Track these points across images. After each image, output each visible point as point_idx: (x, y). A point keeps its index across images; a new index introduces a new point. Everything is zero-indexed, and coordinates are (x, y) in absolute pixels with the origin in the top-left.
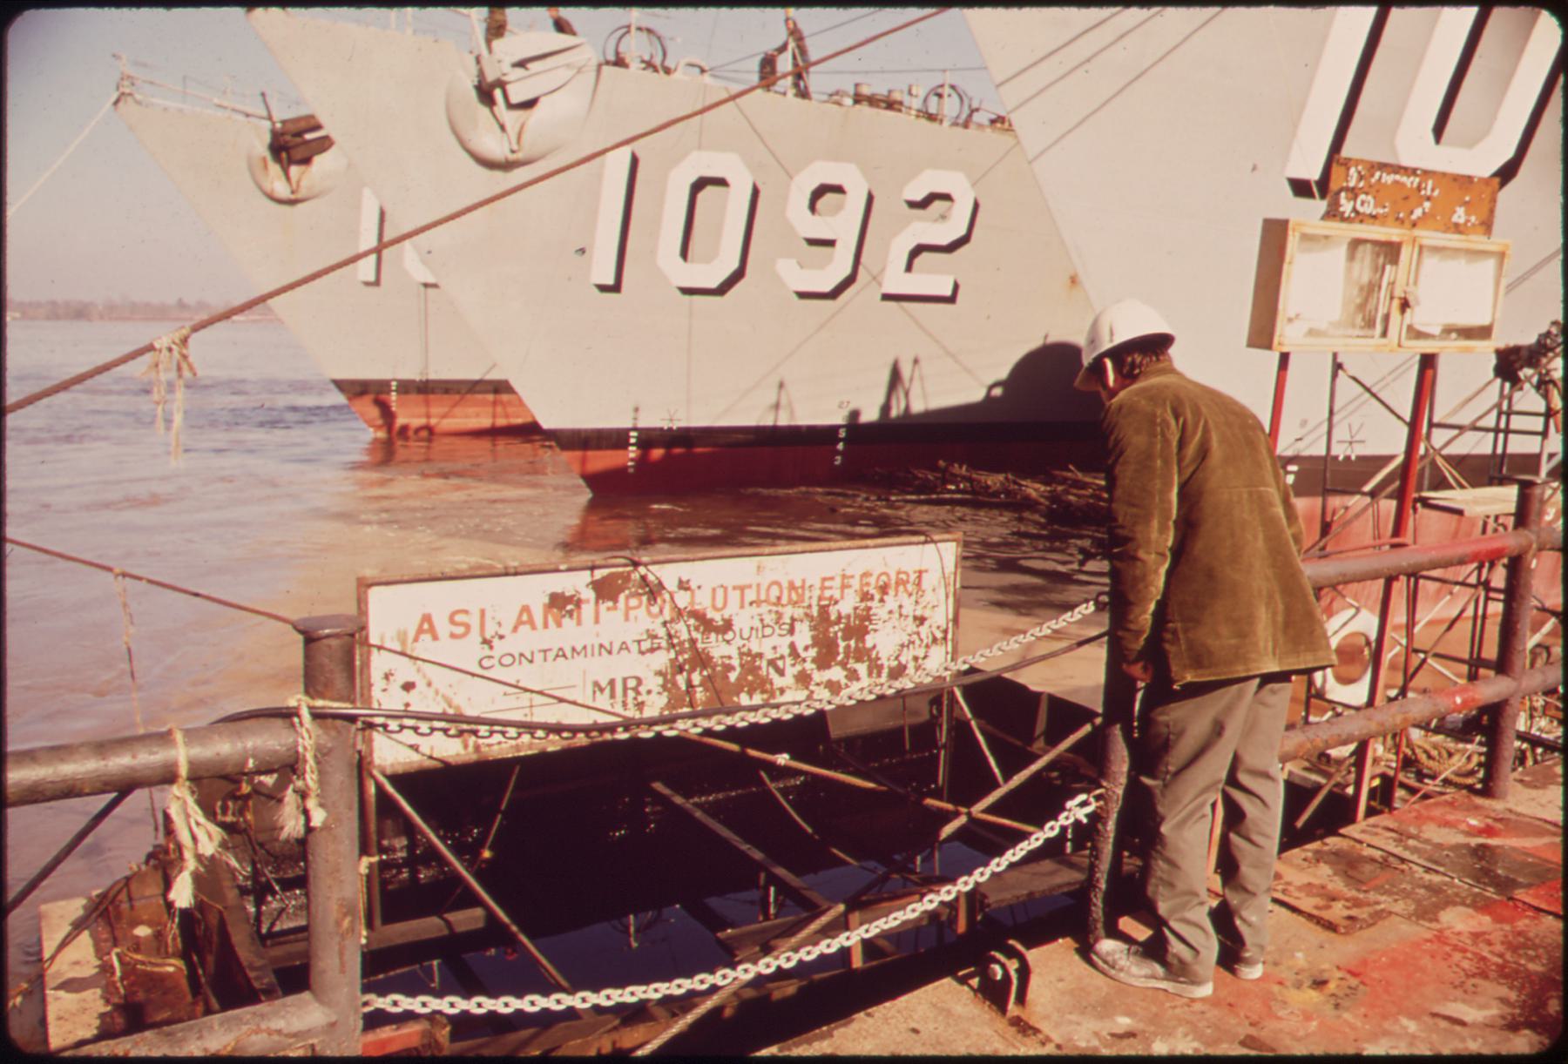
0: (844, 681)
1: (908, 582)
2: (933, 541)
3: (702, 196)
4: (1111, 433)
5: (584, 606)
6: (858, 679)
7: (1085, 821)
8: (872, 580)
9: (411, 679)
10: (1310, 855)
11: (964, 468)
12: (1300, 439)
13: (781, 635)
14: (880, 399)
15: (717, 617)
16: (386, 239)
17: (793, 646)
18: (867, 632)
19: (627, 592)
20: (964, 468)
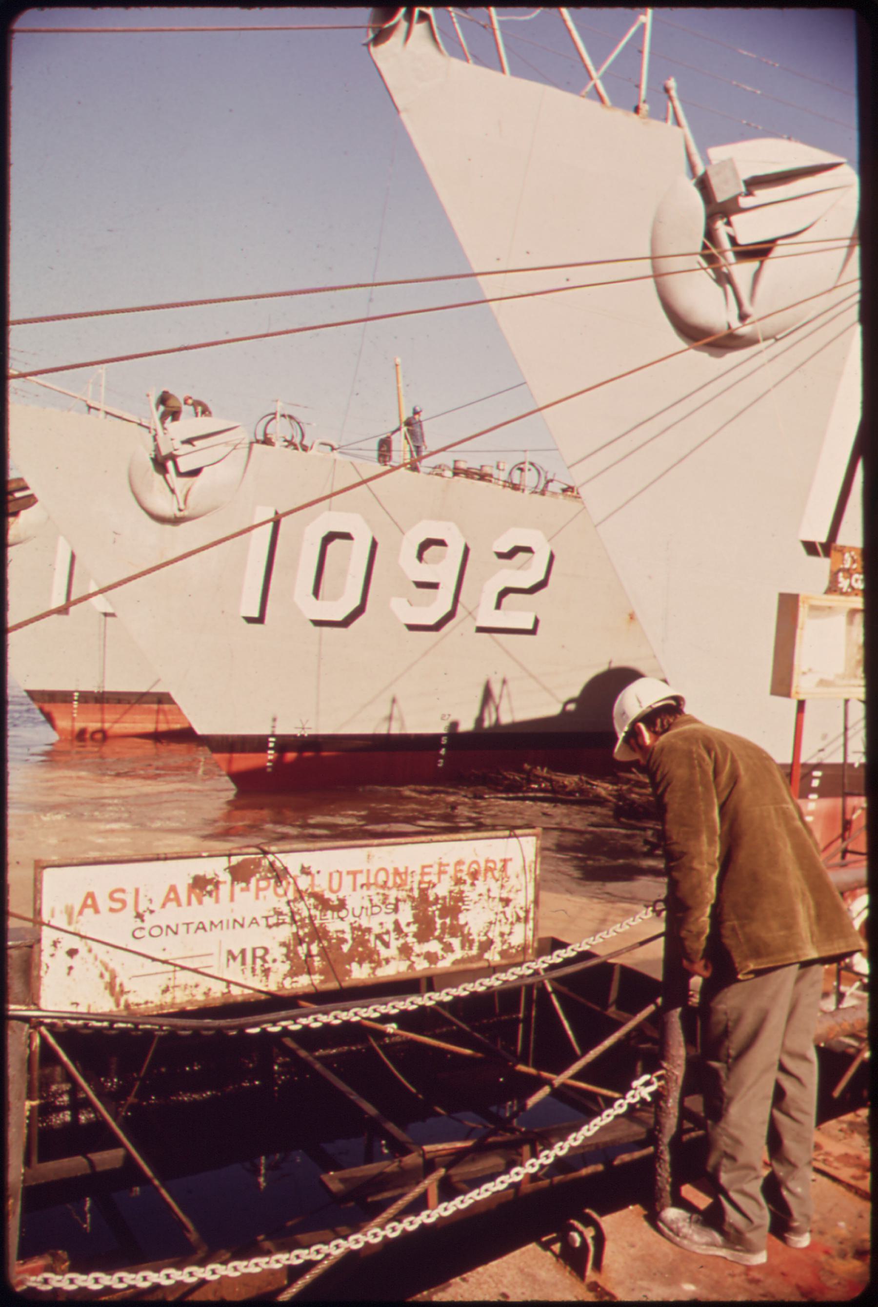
0: (440, 953)
1: (495, 869)
2: (516, 836)
3: (331, 547)
4: (657, 769)
5: (221, 886)
6: (453, 951)
7: (649, 1099)
8: (465, 868)
9: (75, 947)
10: (845, 1126)
11: (545, 770)
12: (822, 750)
13: (387, 913)
14: (476, 713)
15: (334, 898)
16: (73, 598)
17: (397, 923)
18: (461, 911)
19: (258, 876)
20: (545, 770)
